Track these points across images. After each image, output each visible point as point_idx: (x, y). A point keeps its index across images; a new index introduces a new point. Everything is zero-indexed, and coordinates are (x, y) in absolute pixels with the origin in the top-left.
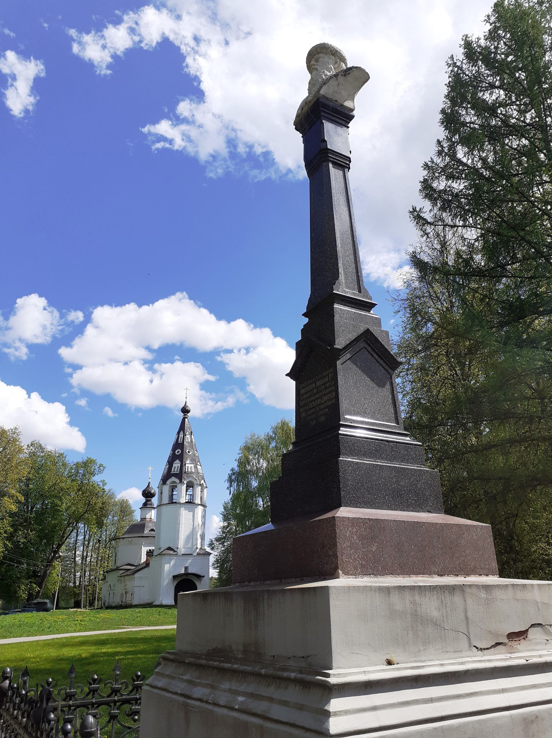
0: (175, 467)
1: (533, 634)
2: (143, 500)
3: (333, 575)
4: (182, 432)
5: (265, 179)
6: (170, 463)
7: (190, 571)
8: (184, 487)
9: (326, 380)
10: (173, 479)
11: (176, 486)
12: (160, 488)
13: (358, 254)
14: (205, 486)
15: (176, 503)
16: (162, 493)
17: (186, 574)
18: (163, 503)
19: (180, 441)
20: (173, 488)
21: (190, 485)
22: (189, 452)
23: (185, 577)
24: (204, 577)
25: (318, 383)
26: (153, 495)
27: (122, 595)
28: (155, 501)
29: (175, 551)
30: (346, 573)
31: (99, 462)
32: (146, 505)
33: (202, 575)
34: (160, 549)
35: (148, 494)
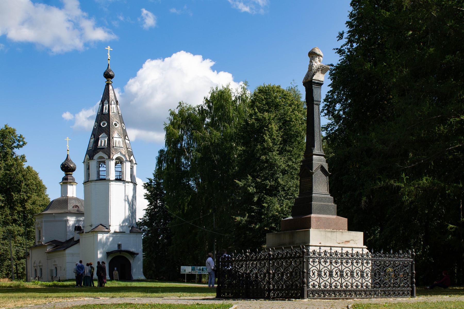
1: (351, 242)
2: (63, 174)
4: (106, 102)
7: (123, 248)
8: (112, 163)
10: (100, 154)
14: (134, 162)
15: (105, 179)
16: (89, 169)
17: (120, 251)
18: (90, 179)
19: (105, 111)
21: (120, 161)
22: (116, 125)
23: (118, 254)
24: (138, 254)
27: (52, 271)
29: (107, 229)
31: (18, 133)
32: (66, 181)
33: (136, 252)
34: (91, 226)
35: (67, 168)
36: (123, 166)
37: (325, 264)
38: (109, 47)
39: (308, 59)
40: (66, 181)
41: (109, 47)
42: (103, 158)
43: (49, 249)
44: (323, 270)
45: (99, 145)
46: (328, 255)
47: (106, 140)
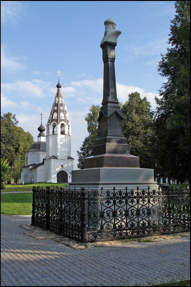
0: (55, 116)
2: (39, 132)
3: (102, 166)
5: (62, 144)
6: (52, 114)
9: (105, 124)
10: (54, 122)
11: (55, 126)
12: (48, 126)
13: (111, 154)
16: (48, 129)
20: (54, 126)
25: (104, 124)
26: (44, 130)
28: (45, 133)
30: (105, 166)
35: (41, 130)
36: (64, 128)
37: (108, 205)
38: (59, 72)
39: (104, 27)
40: (40, 136)
41: (59, 72)
42: (55, 124)
43: (30, 167)
44: (106, 211)
45: (53, 118)
46: (112, 195)
47: (57, 115)
